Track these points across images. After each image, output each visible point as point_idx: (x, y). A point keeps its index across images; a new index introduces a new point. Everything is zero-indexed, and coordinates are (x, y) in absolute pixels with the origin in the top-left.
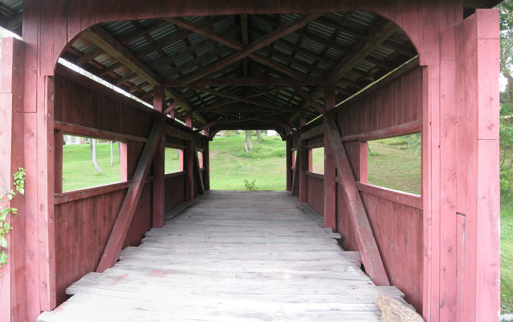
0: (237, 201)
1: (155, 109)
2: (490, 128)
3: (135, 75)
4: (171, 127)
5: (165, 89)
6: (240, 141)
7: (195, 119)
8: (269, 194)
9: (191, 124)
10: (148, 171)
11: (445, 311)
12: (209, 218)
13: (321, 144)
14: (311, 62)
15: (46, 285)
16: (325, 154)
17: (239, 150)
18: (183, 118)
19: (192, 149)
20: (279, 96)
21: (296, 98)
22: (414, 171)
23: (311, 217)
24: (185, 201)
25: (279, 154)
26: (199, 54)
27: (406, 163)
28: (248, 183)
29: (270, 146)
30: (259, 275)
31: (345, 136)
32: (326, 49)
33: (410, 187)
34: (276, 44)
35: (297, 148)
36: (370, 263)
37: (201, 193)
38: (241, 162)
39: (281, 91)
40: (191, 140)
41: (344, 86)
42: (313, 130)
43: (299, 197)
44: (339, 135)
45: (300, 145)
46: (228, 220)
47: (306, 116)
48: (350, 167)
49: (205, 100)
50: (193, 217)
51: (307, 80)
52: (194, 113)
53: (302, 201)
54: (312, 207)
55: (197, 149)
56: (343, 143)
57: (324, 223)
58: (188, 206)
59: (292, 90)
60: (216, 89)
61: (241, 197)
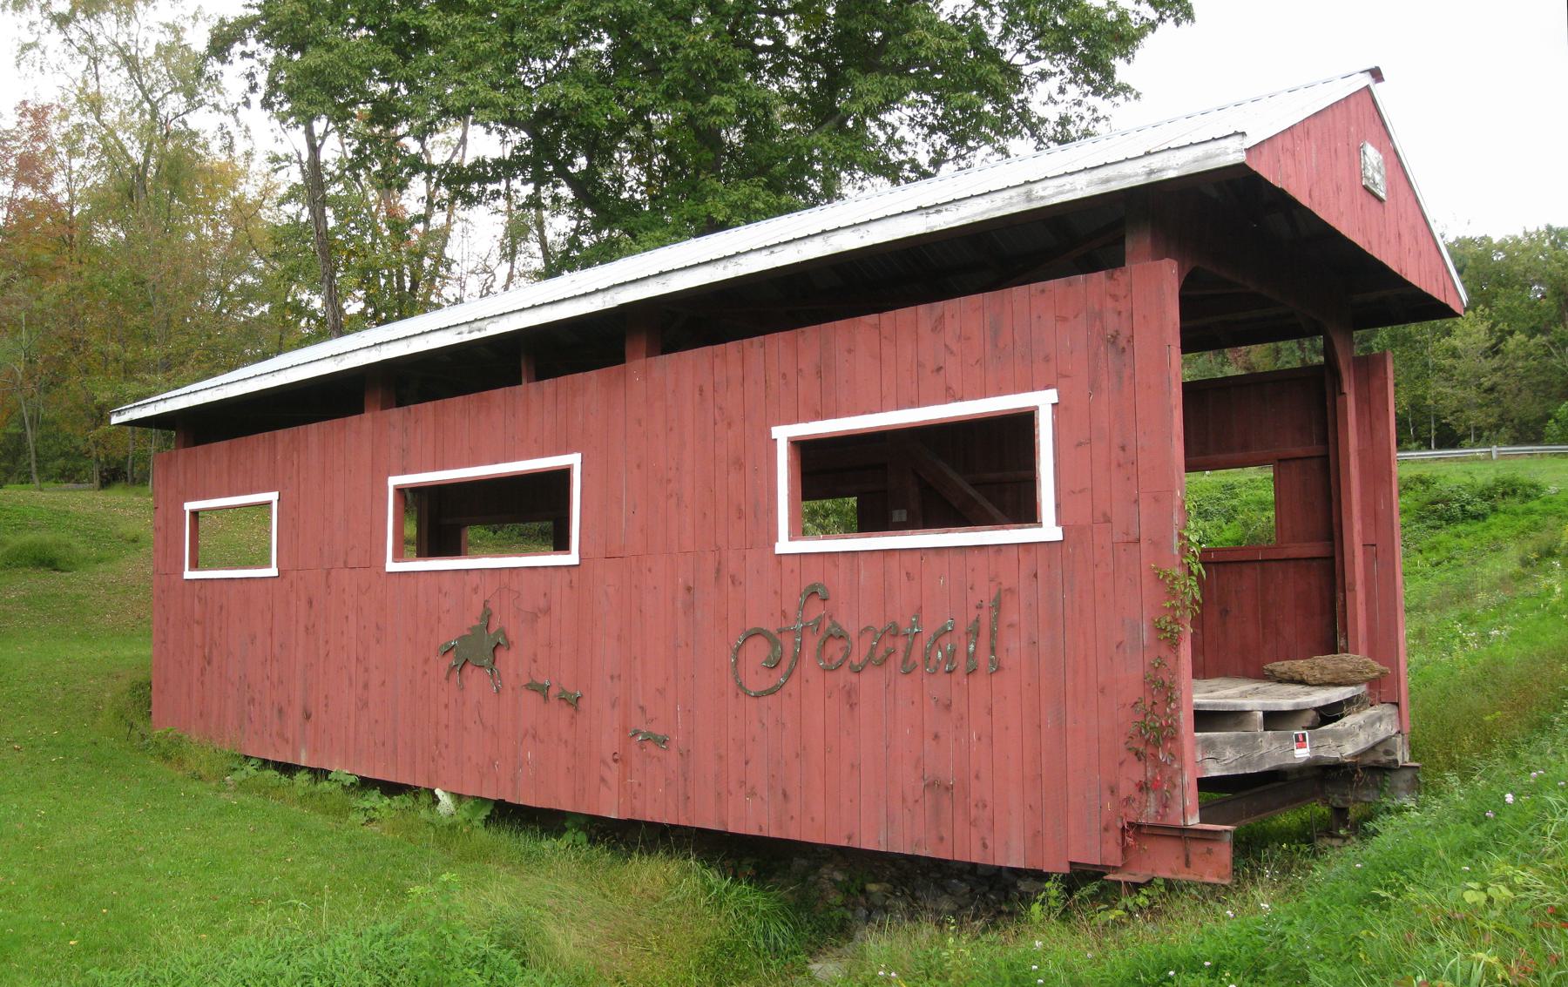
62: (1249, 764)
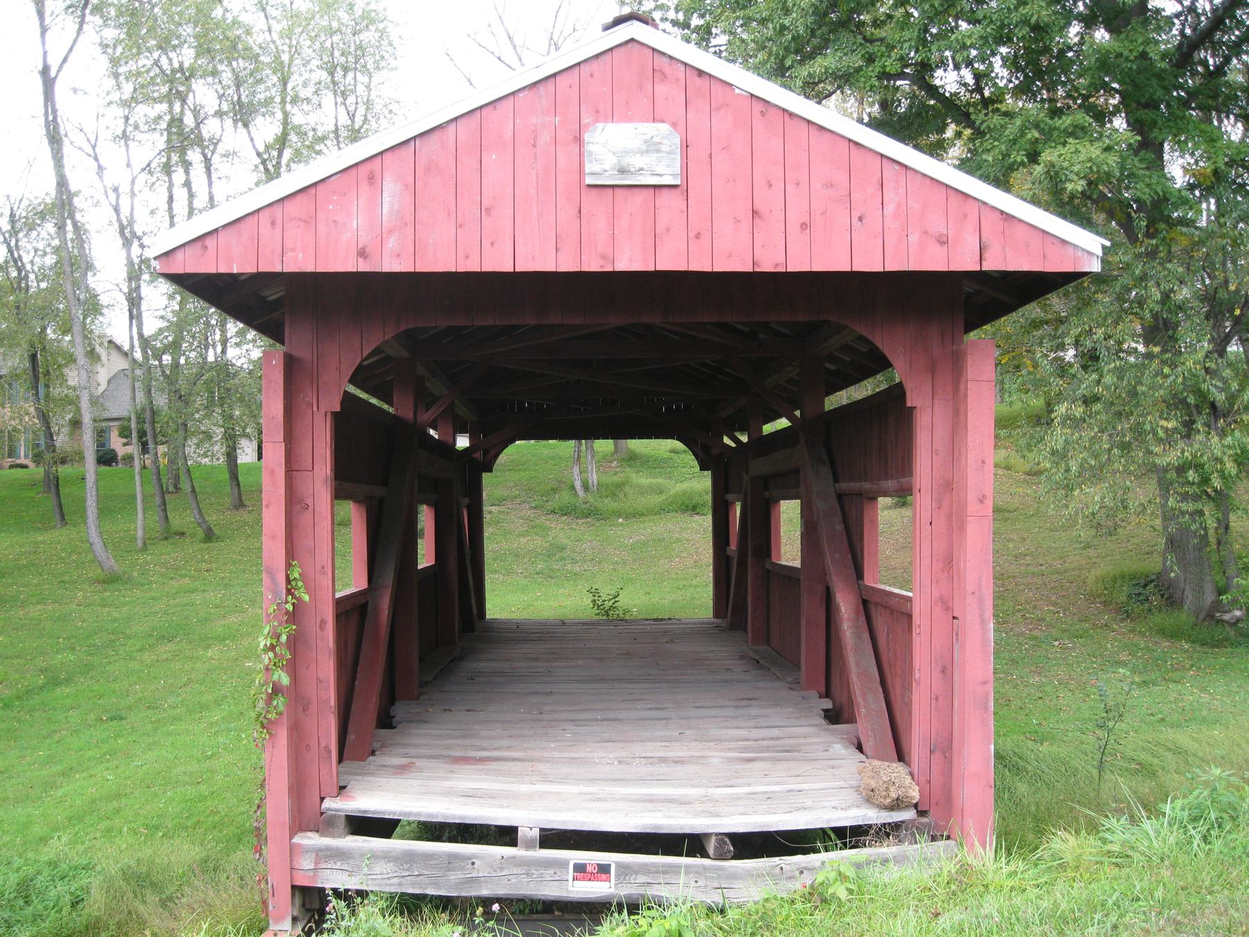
2: (981, 501)
6: (552, 458)
11: (937, 757)
15: (329, 752)
17: (554, 490)
22: (1078, 558)
25: (688, 502)
27: (1064, 534)
29: (656, 477)
30: (663, 760)
33: (1055, 604)
36: (870, 733)
38: (561, 531)
56: (840, 497)
62: (436, 885)
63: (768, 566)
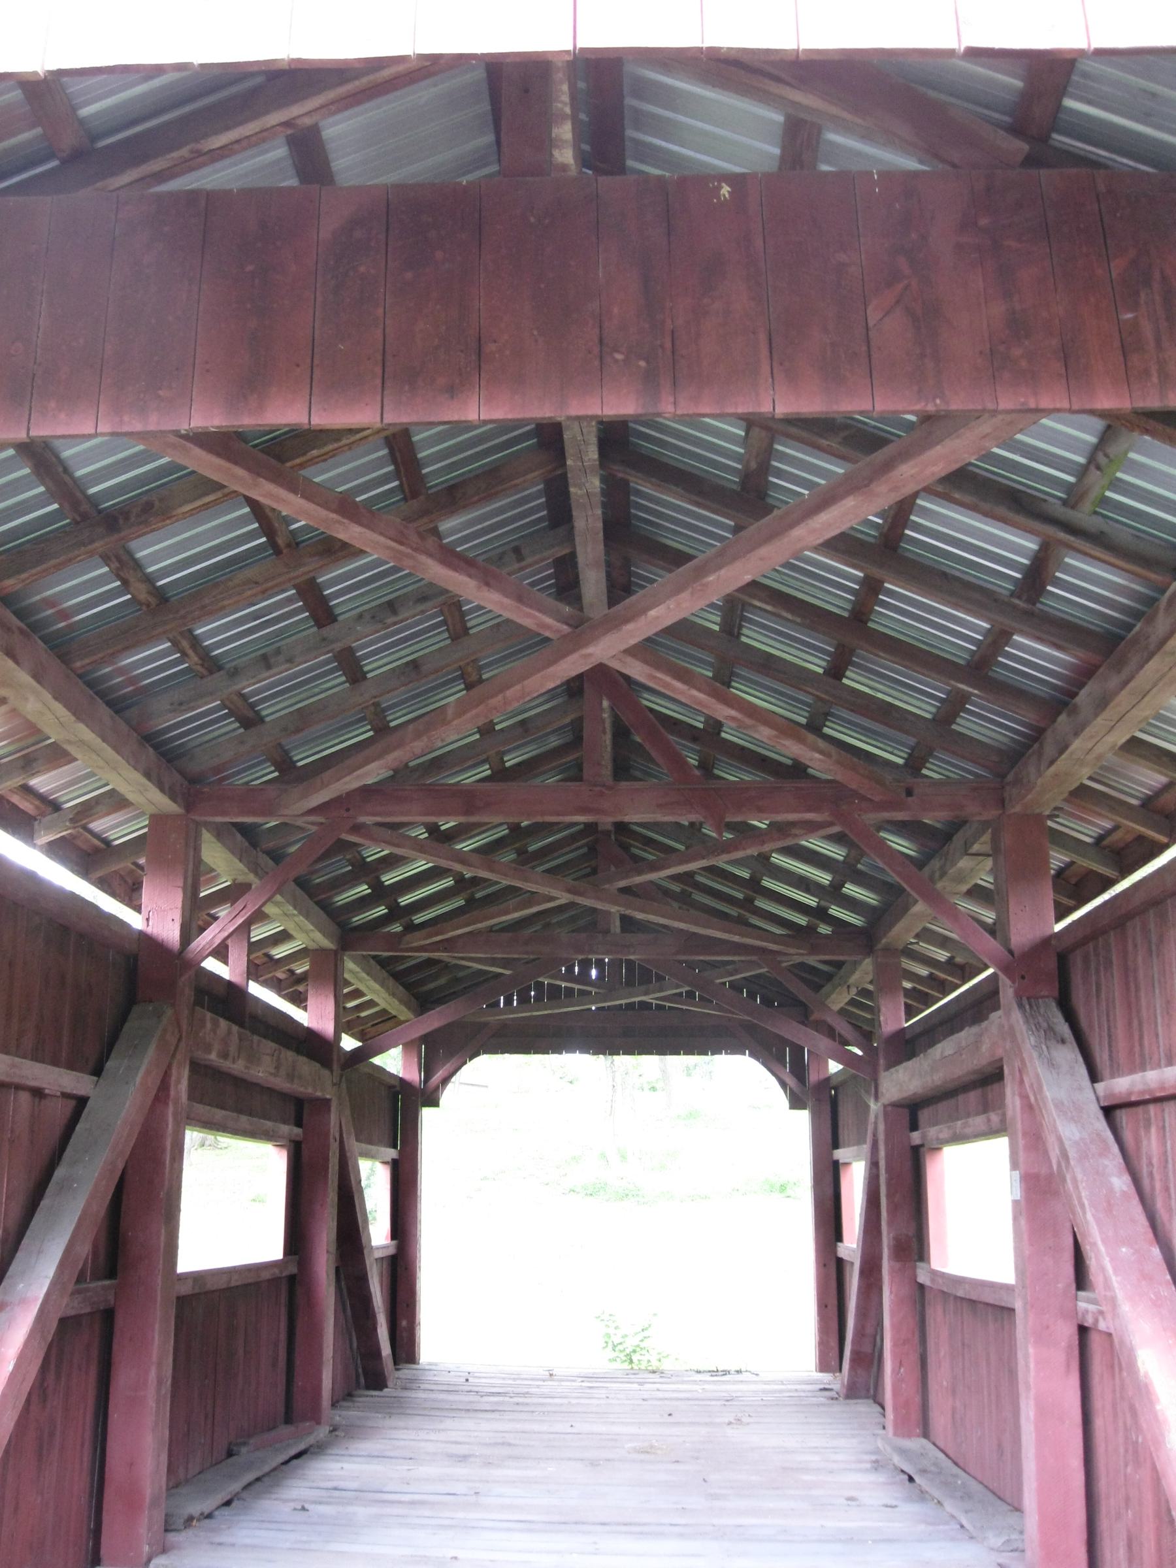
0: (559, 1427)
1: (149, 930)
3: (58, 756)
4: (223, 1023)
5: (204, 831)
7: (357, 993)
8: (724, 1387)
9: (332, 1015)
10: (84, 1250)
12: (402, 1516)
13: (989, 1120)
14: (924, 706)
16: (1017, 1174)
18: (301, 988)
19: (334, 1147)
20: (768, 883)
21: (851, 889)
23: (953, 1517)
24: (288, 1419)
26: (375, 667)
28: (616, 1328)
31: (1113, 1076)
32: (998, 639)
34: (750, 621)
35: (866, 1148)
37: (376, 1380)
39: (778, 859)
40: (328, 1097)
41: (1085, 830)
42: (945, 1048)
43: (883, 1408)
44: (1082, 1071)
45: (881, 1127)
46: (509, 1530)
47: (908, 985)
48: (1151, 1235)
49: (405, 900)
50: (322, 1509)
51: (909, 792)
52: (349, 965)
53: (902, 1428)
54: (956, 1464)
55: (364, 1146)
56: (1109, 1111)
57: (1028, 1554)
58: (302, 1447)
59: (836, 852)
60: (466, 846)
61: (582, 1401)
63: (923, 1278)
